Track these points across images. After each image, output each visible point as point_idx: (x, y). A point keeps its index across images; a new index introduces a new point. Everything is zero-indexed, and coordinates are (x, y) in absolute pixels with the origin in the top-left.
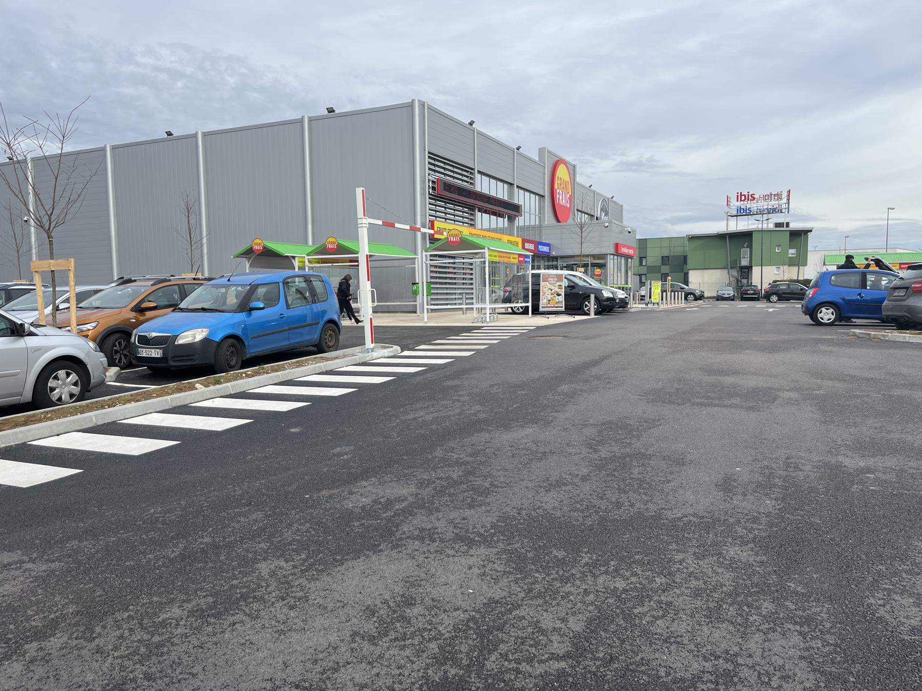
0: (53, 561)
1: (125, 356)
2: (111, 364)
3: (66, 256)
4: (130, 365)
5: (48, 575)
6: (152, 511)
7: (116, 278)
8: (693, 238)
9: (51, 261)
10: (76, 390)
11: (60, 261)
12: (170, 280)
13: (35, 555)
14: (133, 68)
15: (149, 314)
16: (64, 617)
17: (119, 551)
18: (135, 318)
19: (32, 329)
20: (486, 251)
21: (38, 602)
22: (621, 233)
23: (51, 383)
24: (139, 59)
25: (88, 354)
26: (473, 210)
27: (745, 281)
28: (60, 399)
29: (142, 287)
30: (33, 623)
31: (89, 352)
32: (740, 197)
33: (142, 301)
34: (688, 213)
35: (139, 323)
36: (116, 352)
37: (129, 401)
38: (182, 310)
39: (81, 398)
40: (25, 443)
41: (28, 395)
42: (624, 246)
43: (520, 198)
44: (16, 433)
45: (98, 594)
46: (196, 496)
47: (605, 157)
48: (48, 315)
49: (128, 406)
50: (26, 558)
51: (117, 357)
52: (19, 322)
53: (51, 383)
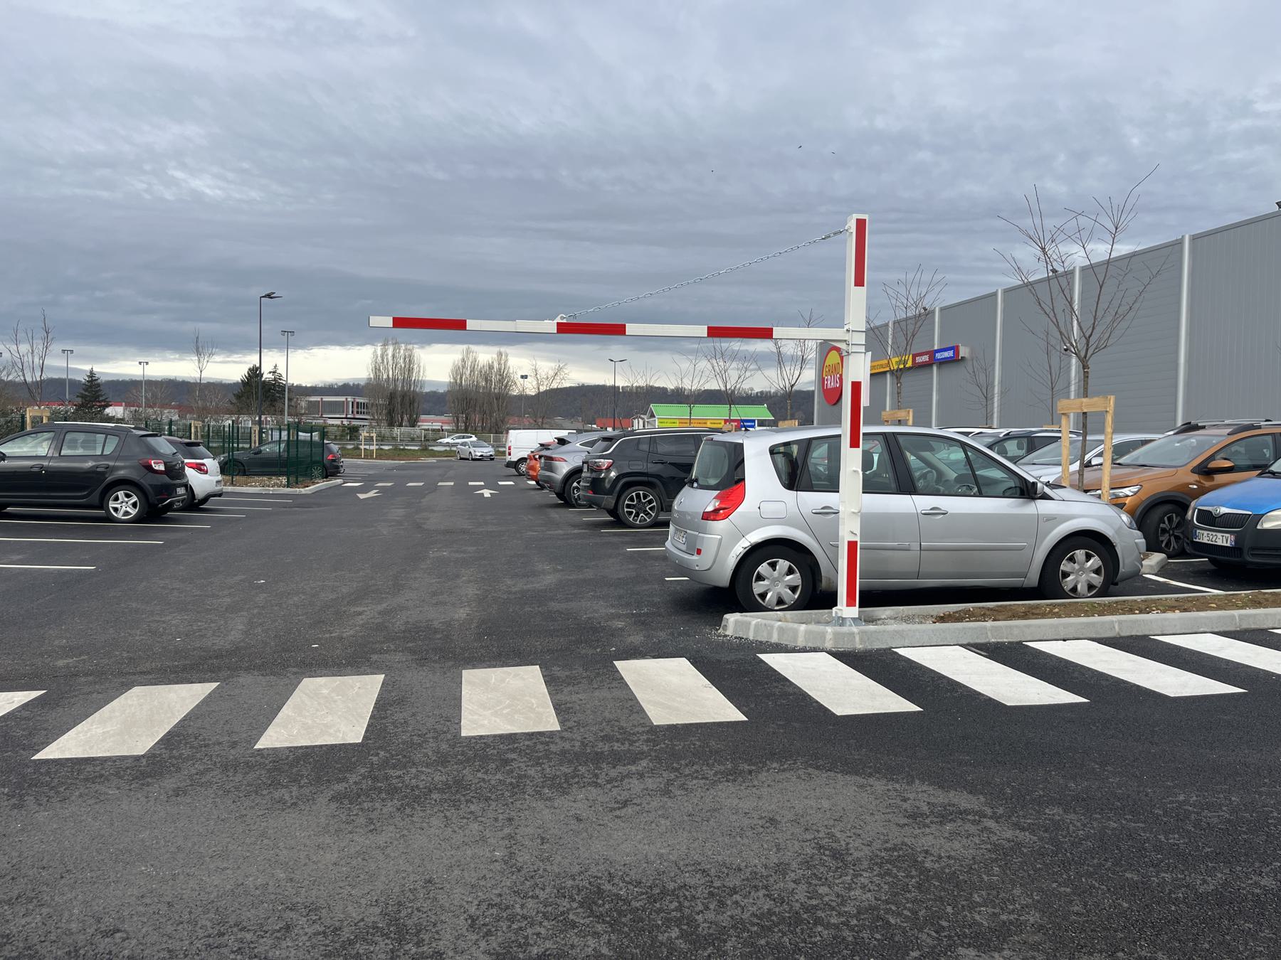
0: (1023, 829)
1: (1177, 538)
2: (1152, 547)
3: (1104, 393)
4: (1182, 554)
5: (1012, 849)
6: (1181, 798)
7: (1179, 423)
9: (1085, 400)
10: (1097, 580)
11: (1095, 399)
12: (1259, 427)
13: (1000, 811)
14: (1247, 123)
15: (1219, 478)
16: (1020, 925)
17: (1119, 848)
18: (1197, 483)
19: (1047, 490)
21: (991, 887)
23: (1065, 566)
24: (1261, 107)
25: (1118, 531)
28: (1074, 589)
29: (1213, 437)
30: (977, 917)
31: (1120, 528)
33: (1212, 458)
35: (1203, 491)
36: (1164, 531)
37: (1172, 609)
38: (1274, 475)
39: (1103, 592)
40: (1020, 643)
41: (1033, 579)
44: (1010, 627)
45: (1076, 908)
46: (1260, 794)
48: (1074, 473)
49: (1169, 615)
50: (989, 811)
51: (1165, 538)
52: (1031, 480)
53: (1065, 566)
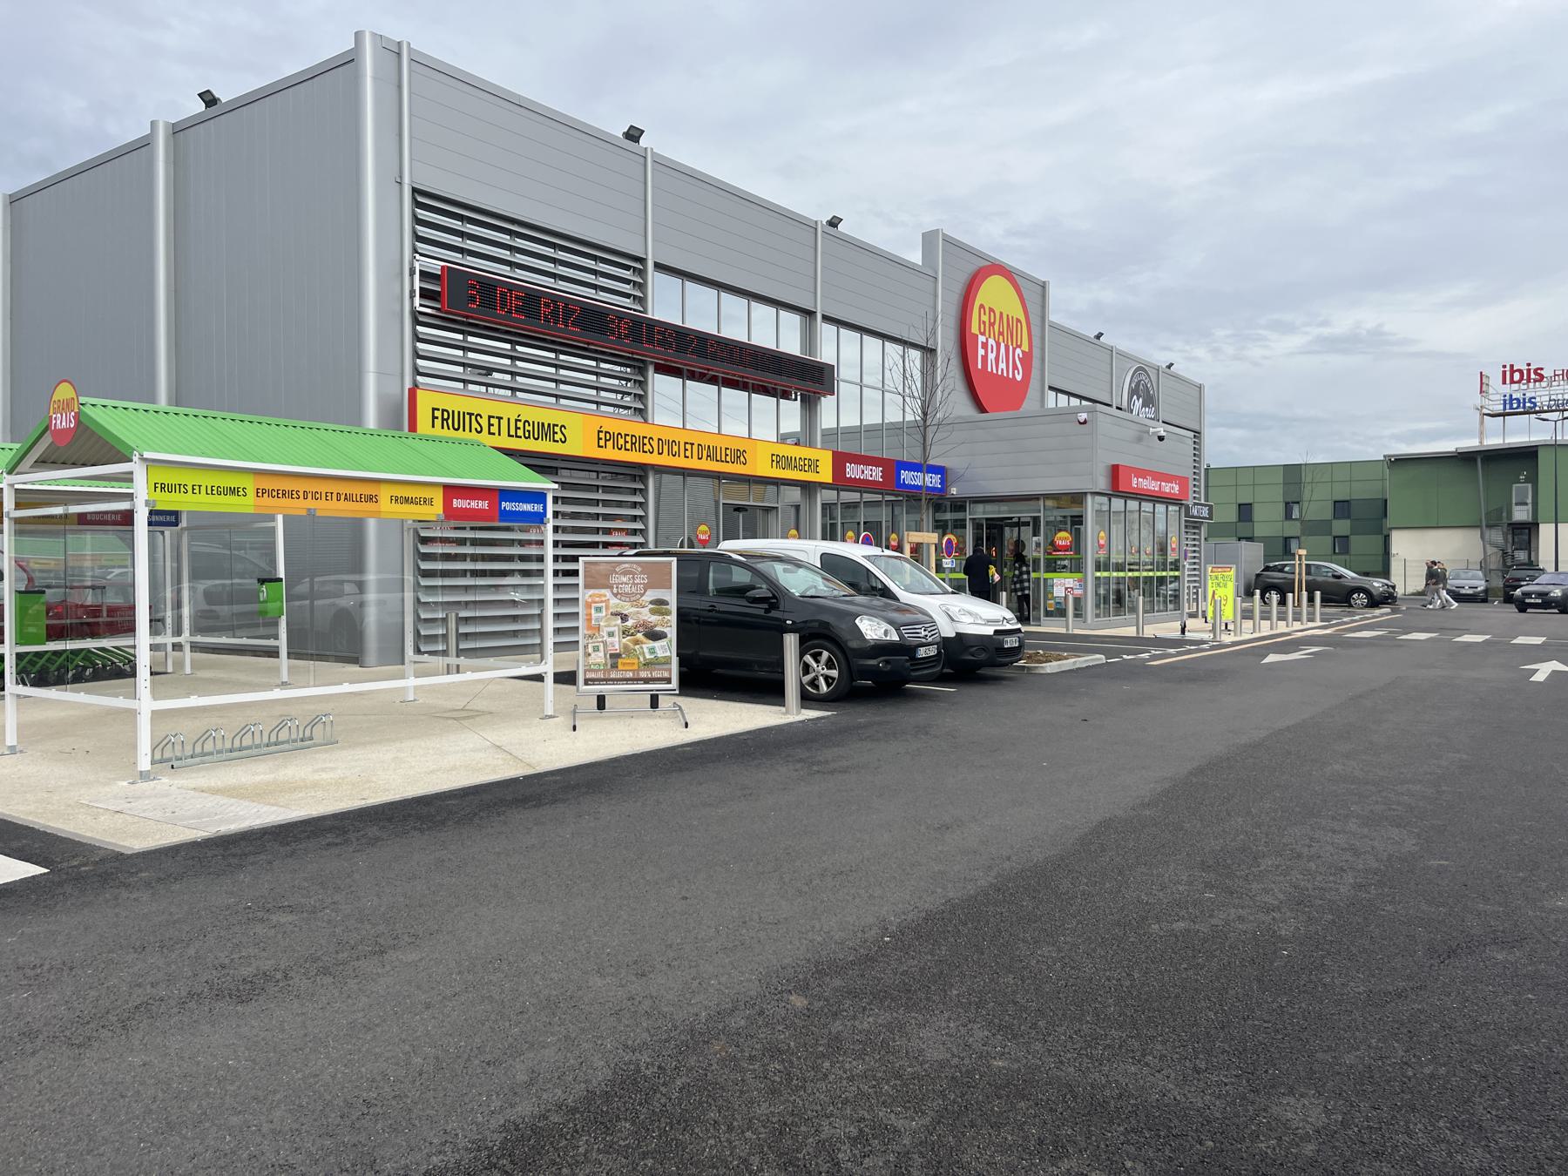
8: (1399, 462)
20: (136, 468)
22: (1139, 440)
26: (642, 370)
27: (1521, 556)
32: (1510, 374)
34: (1442, 424)
42: (1143, 473)
43: (831, 347)
47: (1287, 329)
